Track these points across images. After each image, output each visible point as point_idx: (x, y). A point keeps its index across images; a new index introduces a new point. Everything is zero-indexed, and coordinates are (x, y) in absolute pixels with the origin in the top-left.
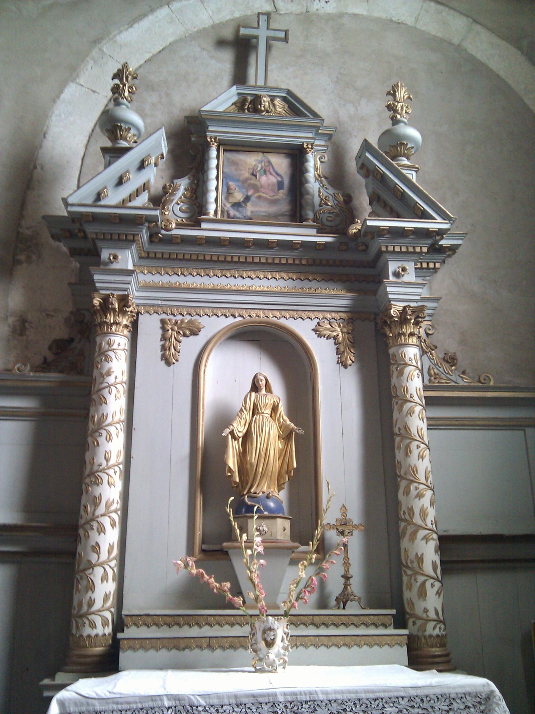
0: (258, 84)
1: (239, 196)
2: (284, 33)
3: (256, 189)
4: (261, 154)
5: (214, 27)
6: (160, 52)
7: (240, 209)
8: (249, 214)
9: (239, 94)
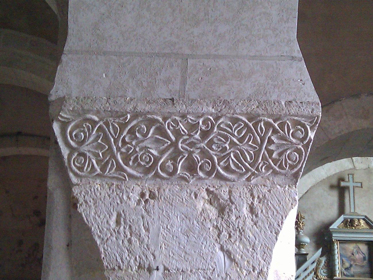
0: (352, 211)
1: (347, 265)
2: (360, 184)
3: (354, 261)
4: (355, 244)
5: (328, 178)
6: (306, 193)
7: (348, 271)
8: (352, 273)
9: (344, 218)
